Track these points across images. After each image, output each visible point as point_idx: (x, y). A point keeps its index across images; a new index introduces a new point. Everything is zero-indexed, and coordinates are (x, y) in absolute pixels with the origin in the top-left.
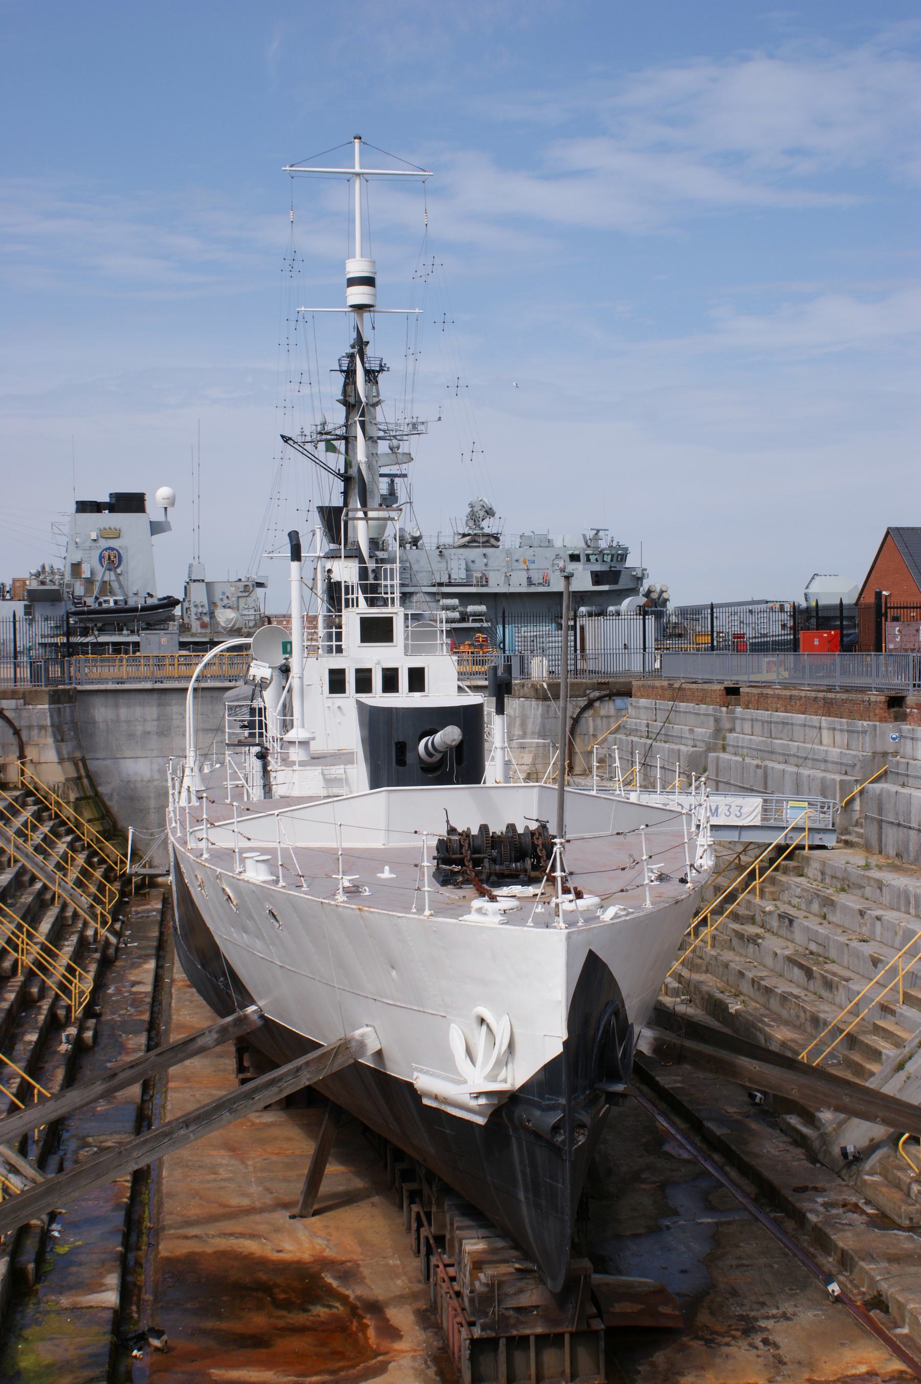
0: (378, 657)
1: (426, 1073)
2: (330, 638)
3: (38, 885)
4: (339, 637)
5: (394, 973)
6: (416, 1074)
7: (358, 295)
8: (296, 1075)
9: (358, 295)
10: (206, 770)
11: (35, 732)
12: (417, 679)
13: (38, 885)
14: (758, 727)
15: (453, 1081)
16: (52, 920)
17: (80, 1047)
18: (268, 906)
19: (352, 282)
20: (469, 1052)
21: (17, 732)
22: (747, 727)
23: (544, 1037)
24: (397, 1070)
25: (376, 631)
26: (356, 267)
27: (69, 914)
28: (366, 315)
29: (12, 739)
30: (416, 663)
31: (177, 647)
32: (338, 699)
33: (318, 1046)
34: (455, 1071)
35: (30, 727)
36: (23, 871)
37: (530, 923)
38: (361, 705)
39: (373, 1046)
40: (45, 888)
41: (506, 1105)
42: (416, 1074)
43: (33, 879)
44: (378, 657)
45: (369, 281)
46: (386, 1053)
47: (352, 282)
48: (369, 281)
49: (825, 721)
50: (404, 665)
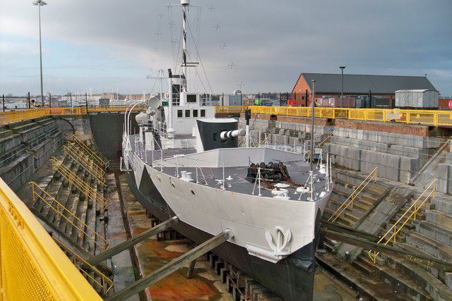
0: (197, 106)
4: (179, 100)
12: (203, 113)
15: (268, 250)
20: (273, 241)
24: (240, 243)
30: (203, 108)
31: (195, 109)
32: (180, 119)
33: (209, 236)
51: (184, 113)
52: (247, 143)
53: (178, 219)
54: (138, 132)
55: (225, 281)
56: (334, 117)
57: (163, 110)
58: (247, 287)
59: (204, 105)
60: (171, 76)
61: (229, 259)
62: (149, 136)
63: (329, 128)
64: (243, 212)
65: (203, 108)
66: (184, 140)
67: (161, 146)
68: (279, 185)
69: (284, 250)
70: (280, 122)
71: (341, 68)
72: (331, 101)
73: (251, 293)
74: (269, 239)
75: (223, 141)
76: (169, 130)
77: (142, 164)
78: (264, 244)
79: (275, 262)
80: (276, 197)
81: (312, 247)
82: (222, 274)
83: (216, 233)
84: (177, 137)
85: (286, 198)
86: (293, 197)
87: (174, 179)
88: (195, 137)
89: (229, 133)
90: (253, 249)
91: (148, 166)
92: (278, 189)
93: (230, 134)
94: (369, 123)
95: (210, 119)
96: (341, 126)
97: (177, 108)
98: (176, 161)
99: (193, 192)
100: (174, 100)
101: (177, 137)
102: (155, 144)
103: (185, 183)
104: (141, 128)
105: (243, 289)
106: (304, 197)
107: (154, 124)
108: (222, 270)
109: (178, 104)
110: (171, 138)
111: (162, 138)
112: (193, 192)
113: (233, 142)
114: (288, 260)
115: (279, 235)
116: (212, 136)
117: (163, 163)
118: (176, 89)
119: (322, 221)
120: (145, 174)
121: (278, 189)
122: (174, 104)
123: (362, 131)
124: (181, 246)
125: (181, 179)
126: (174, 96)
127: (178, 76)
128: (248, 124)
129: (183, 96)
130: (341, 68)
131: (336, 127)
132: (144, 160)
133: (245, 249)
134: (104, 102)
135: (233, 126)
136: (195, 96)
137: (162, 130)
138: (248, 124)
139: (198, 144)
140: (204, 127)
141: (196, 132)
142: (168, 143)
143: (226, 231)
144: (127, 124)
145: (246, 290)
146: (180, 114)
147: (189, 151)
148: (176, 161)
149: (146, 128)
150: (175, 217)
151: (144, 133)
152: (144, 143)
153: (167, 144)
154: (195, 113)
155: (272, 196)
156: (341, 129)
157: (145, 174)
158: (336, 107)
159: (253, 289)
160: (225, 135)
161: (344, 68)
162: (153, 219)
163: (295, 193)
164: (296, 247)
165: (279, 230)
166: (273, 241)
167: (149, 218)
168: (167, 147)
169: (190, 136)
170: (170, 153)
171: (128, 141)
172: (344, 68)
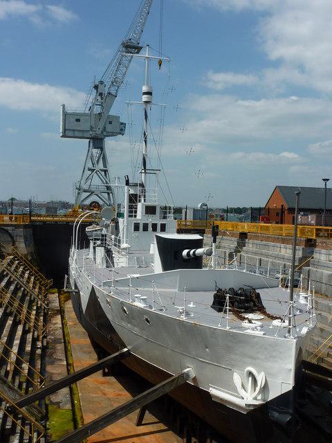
0: (150, 220)
3: (23, 289)
4: (136, 212)
5: (207, 350)
6: (211, 389)
7: (145, 98)
8: (160, 388)
9: (145, 98)
10: (263, 357)
11: (18, 237)
12: (163, 228)
13: (23, 289)
14: (255, 246)
15: (235, 396)
16: (6, 281)
17: (44, 349)
18: (146, 317)
19: (145, 93)
20: (243, 386)
21: (12, 237)
22: (251, 246)
23: (283, 382)
26: (145, 89)
27: (32, 299)
29: (9, 239)
30: (164, 222)
32: (137, 233)
34: (237, 392)
35: (17, 236)
36: (18, 284)
38: (159, 239)
39: (193, 375)
40: (25, 290)
41: (261, 413)
42: (211, 389)
43: (21, 287)
44: (150, 220)
45: (149, 93)
47: (145, 93)
48: (149, 93)
49: (282, 245)
50: (159, 222)
51: (141, 227)
54: (88, 246)
57: (117, 223)
60: (127, 183)
61: (184, 407)
63: (308, 250)
67: (113, 263)
68: (250, 316)
69: (255, 399)
70: (251, 241)
72: (311, 219)
76: (124, 245)
78: (232, 388)
88: (153, 255)
89: (193, 250)
93: (194, 252)
96: (323, 248)
100: (131, 212)
102: (107, 261)
104: (92, 245)
109: (135, 216)
111: (115, 255)
113: (196, 262)
115: (250, 378)
116: (173, 255)
118: (133, 199)
121: (250, 321)
126: (130, 207)
127: (136, 185)
129: (140, 207)
133: (208, 394)
135: (198, 244)
137: (115, 245)
138: (215, 241)
139: (157, 266)
141: (154, 249)
142: (121, 260)
146: (137, 228)
150: (126, 350)
151: (94, 248)
154: (154, 227)
156: (323, 251)
160: (188, 253)
161: (328, 180)
164: (273, 395)
165: (250, 374)
172: (328, 180)
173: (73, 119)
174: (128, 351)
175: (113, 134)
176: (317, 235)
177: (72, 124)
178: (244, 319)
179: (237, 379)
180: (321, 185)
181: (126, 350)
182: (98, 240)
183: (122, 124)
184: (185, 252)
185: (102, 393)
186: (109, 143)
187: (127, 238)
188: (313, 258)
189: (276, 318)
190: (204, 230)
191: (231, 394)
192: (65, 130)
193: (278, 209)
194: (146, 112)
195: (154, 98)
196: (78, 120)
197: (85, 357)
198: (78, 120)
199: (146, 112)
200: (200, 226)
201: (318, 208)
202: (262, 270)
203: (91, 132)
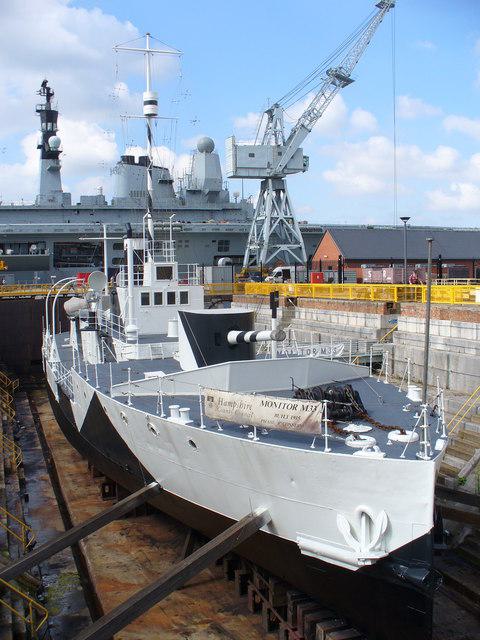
0: (165, 287)
1: (304, 537)
2: (135, 277)
4: (141, 277)
6: (298, 538)
7: (148, 109)
9: (148, 109)
12: (184, 297)
15: (340, 547)
18: (189, 438)
20: (353, 533)
23: (415, 519)
24: (285, 533)
25: (164, 273)
26: (147, 96)
28: (153, 120)
30: (184, 289)
31: (170, 291)
33: (228, 522)
37: (402, 456)
42: (298, 538)
44: (165, 287)
45: (153, 102)
46: (275, 522)
48: (153, 102)
49: (351, 314)
50: (178, 289)
51: (152, 299)
52: (130, 322)
53: (159, 486)
54: (66, 329)
55: (244, 591)
56: (396, 300)
58: (290, 605)
59: (186, 282)
61: (262, 564)
62: (90, 339)
63: (391, 317)
64: (292, 480)
65: (184, 289)
66: (156, 345)
69: (373, 550)
70: (304, 310)
71: (403, 219)
72: (387, 273)
73: (300, 618)
74: (345, 531)
75: (233, 346)
76: (129, 328)
77: (91, 390)
79: (355, 569)
80: (359, 453)
81: (429, 542)
82: (237, 580)
83: (236, 512)
84: (143, 339)
85: (378, 455)
86: (393, 451)
87: (156, 421)
88: (176, 340)
90: (312, 544)
91: (100, 395)
92: (357, 436)
94: (460, 308)
95: (197, 307)
96: (411, 315)
97: (140, 290)
98: (155, 383)
99: (192, 442)
101: (143, 339)
102: (106, 351)
103: (179, 428)
104: (73, 324)
105: (282, 610)
106: (412, 452)
107: (99, 318)
108: (237, 573)
109: (141, 283)
110: (133, 342)
111: (117, 342)
112: (192, 442)
113: (244, 351)
114: (381, 565)
117: (130, 389)
119: (446, 489)
120: (95, 406)
121: (357, 436)
122: (135, 283)
123: (448, 322)
124: (336, 633)
125: (168, 419)
128: (274, 315)
130: (403, 219)
131: (401, 318)
132: (92, 383)
133: (293, 547)
134: (84, 276)
136: (158, 268)
138: (274, 315)
140: (191, 322)
141: (176, 329)
142: (128, 350)
143: (259, 512)
144: (50, 316)
145: (290, 614)
146: (145, 300)
147: (171, 365)
148: (155, 383)
149: (84, 325)
150: (154, 484)
151: (79, 331)
152: (80, 348)
153: (126, 351)
154: (171, 298)
155: (352, 450)
156: (411, 319)
157: (95, 406)
158: (397, 283)
159: (304, 613)
160: (240, 338)
161: (408, 219)
162: (103, 479)
163: (389, 443)
164: (396, 543)
165: (363, 513)
166: (353, 533)
167: (95, 476)
168: (125, 358)
169: (163, 338)
170: (138, 368)
171: (54, 346)
172: (408, 219)
173: (243, 155)
174: (159, 486)
175: (295, 171)
176: (399, 297)
177: (245, 162)
178: (347, 434)
179: (342, 522)
180: (401, 223)
181: (154, 484)
182: (84, 320)
183: (305, 157)
184: (233, 336)
185: (118, 560)
186: (290, 181)
187: (133, 316)
188: (396, 329)
189: (393, 429)
190: (231, 296)
191: (332, 545)
192: (237, 169)
193: (334, 262)
194: (149, 130)
195: (160, 110)
196: (252, 155)
197: (86, 503)
198: (252, 155)
199: (149, 130)
200: (220, 292)
201: (471, 257)
202: (305, 353)
203: (269, 170)
